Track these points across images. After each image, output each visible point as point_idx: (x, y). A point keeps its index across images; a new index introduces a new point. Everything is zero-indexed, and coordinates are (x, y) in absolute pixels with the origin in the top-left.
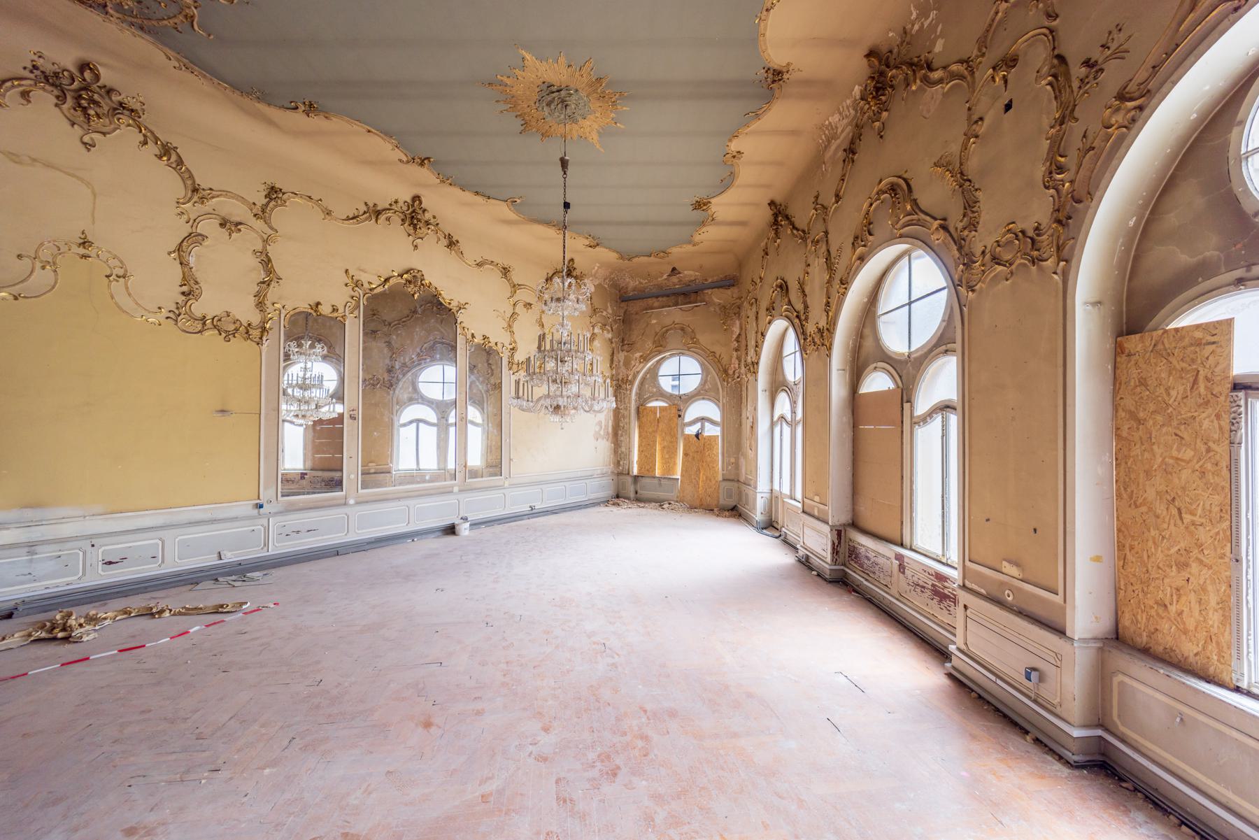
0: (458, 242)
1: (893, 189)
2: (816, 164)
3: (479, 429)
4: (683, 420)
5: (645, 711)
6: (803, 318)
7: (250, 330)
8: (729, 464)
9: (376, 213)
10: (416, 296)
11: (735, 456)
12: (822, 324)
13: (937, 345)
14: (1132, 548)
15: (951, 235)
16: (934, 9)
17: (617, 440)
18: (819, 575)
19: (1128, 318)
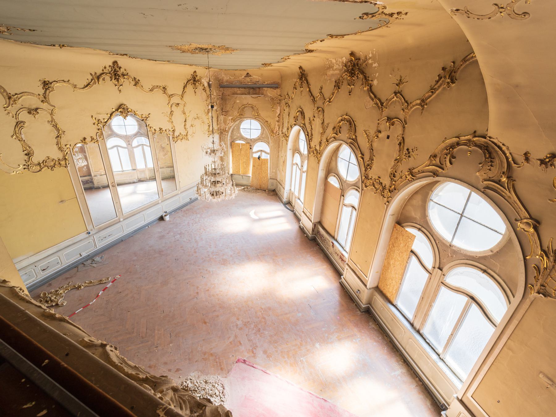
5: (262, 309)
7: (60, 162)
8: (272, 172)
9: (98, 77)
11: (275, 169)
14: (385, 271)
18: (307, 236)
19: (399, 218)
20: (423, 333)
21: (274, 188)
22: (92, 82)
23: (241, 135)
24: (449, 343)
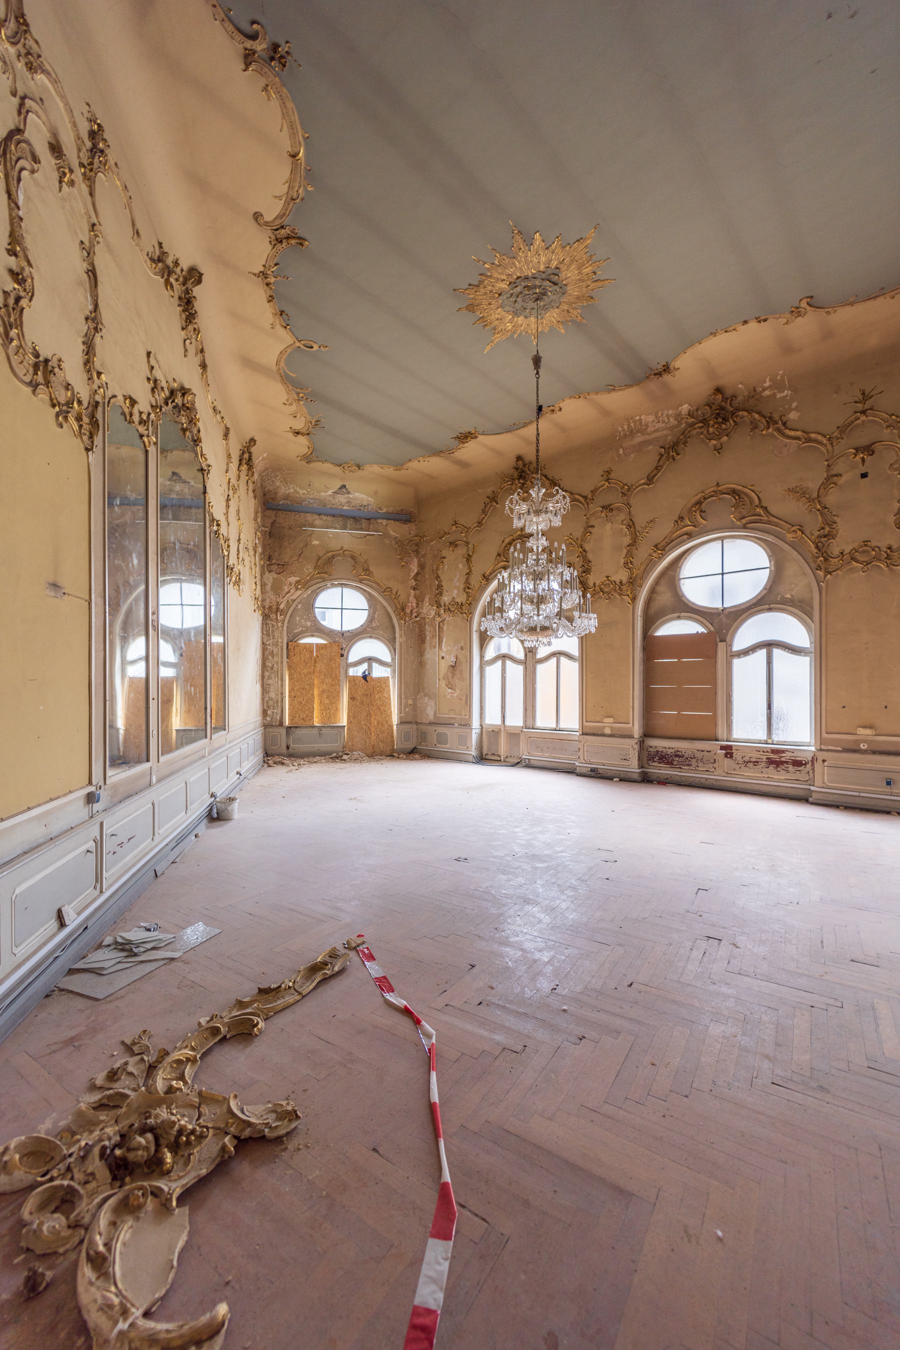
4: (347, 659)
8: (406, 705)
16: (789, 389)
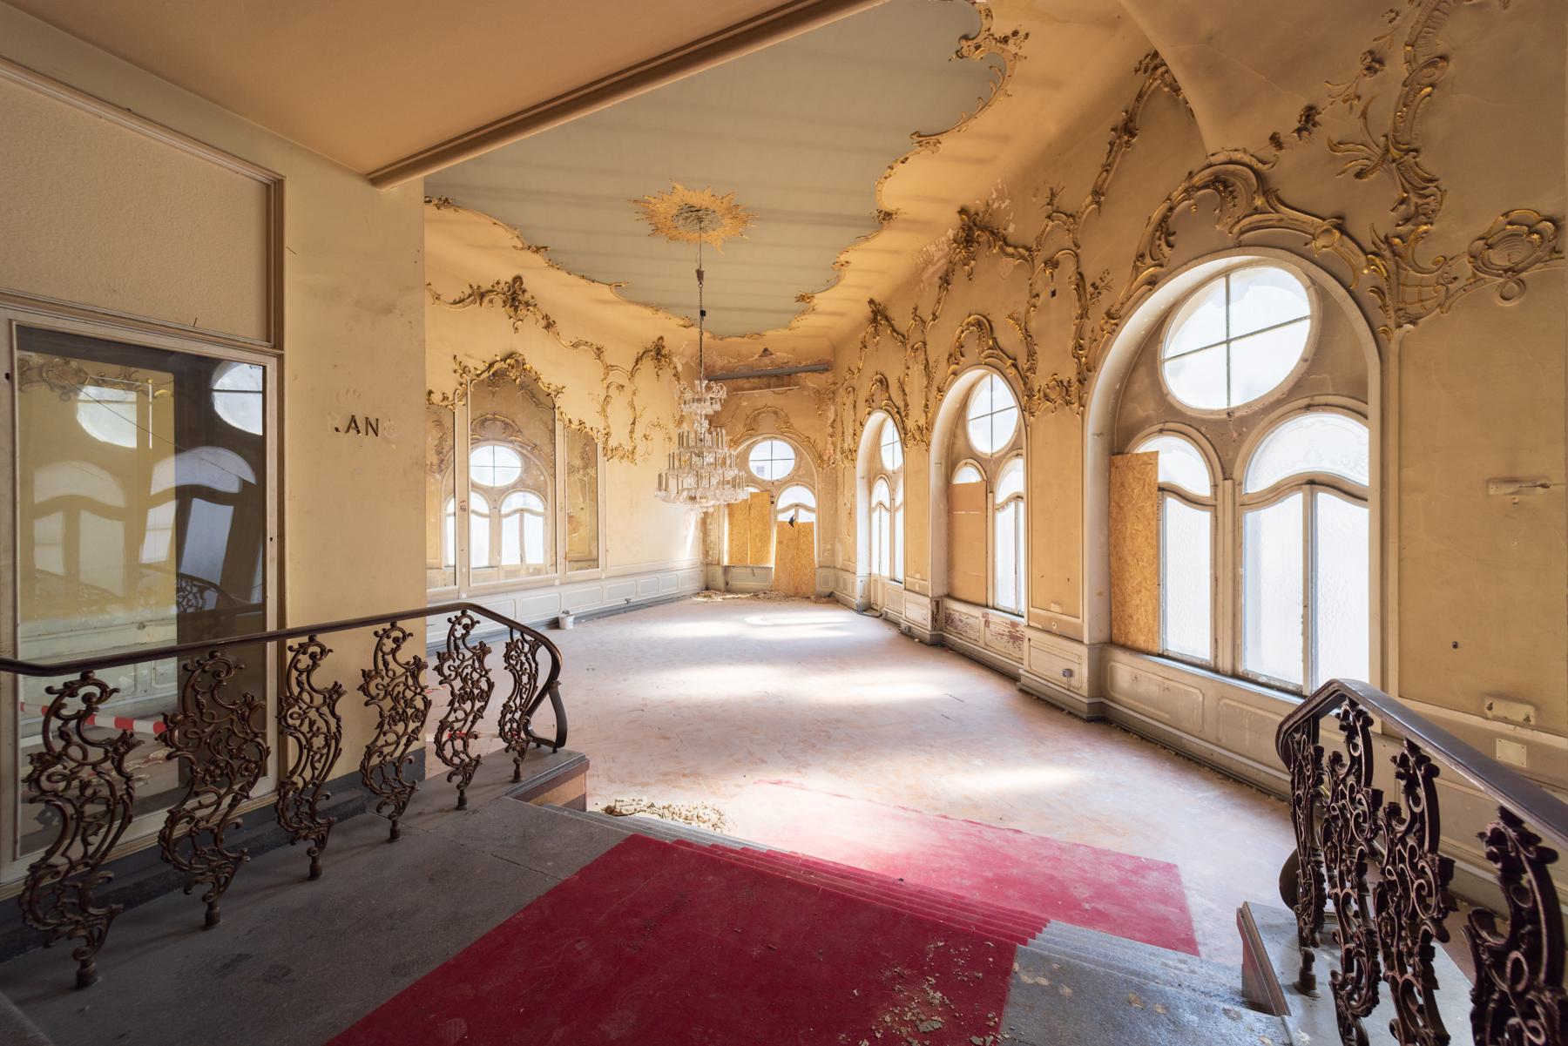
0: (554, 322)
1: (979, 324)
2: (913, 281)
3: (540, 519)
4: (776, 506)
6: (903, 414)
8: (824, 551)
9: (480, 295)
10: (518, 381)
12: (922, 422)
13: (1011, 449)
15: (1020, 373)
17: (705, 529)
18: (920, 642)
20: (1246, 670)
21: (831, 591)
22: (469, 300)
23: (750, 476)
24: (1308, 638)
